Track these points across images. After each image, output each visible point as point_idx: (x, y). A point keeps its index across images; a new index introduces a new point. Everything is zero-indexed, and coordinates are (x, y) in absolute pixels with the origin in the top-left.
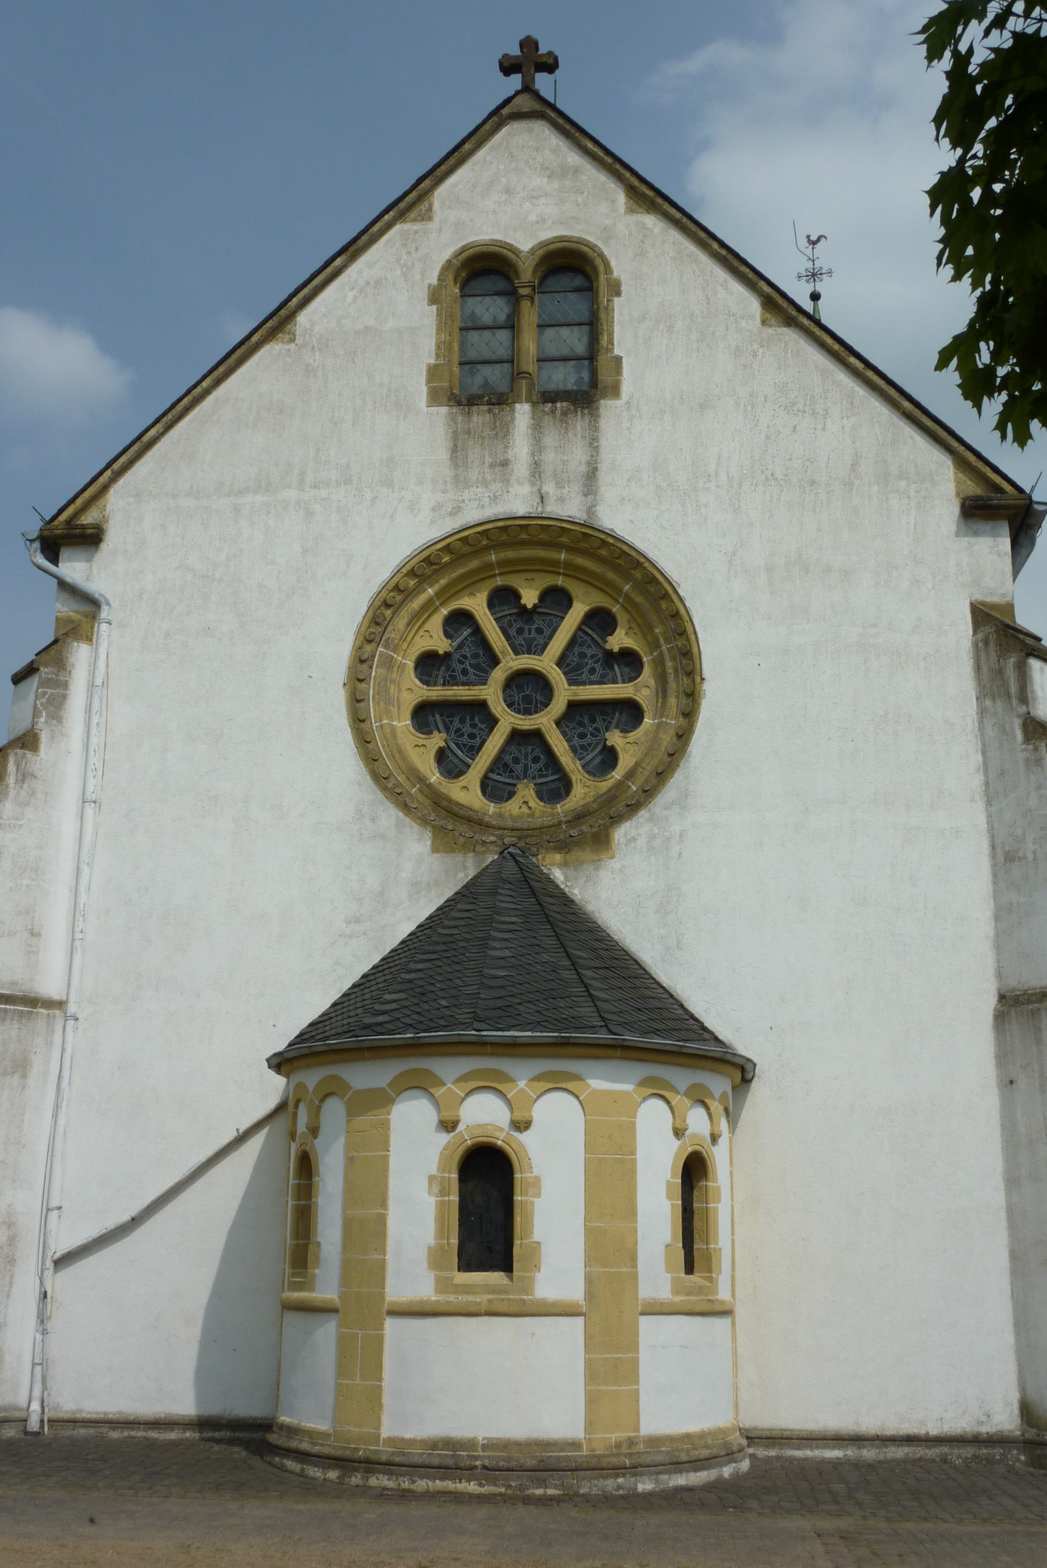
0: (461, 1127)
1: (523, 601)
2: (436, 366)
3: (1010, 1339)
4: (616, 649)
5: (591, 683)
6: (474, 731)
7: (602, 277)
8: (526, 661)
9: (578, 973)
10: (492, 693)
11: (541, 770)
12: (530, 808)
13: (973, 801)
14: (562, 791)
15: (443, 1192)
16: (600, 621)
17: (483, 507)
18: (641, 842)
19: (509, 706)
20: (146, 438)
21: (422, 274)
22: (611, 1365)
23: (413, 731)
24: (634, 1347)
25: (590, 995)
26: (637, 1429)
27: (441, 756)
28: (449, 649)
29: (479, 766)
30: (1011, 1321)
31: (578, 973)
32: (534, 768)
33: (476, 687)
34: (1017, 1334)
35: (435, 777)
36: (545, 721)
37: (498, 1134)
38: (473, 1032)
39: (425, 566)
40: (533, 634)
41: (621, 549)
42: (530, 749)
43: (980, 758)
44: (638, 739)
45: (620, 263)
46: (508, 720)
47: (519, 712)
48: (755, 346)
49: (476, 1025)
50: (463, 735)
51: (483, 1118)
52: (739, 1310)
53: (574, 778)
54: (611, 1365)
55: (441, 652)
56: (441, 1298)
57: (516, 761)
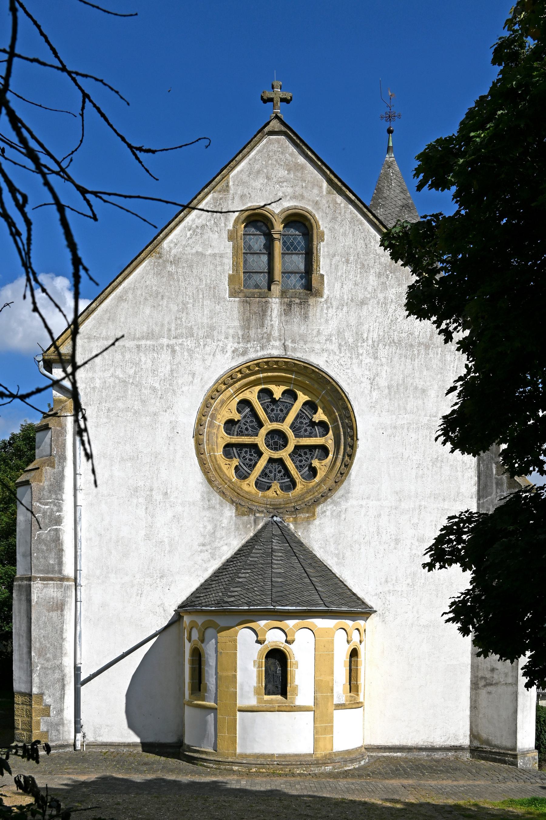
0: (266, 642)
1: (274, 397)
2: (233, 275)
3: (468, 712)
4: (317, 421)
5: (305, 437)
6: (252, 458)
7: (315, 231)
8: (275, 426)
9: (310, 580)
10: (260, 440)
11: (282, 476)
12: (277, 494)
13: (472, 498)
14: (292, 486)
15: (259, 667)
16: (311, 406)
17: (257, 351)
18: (328, 513)
19: (267, 446)
20: (90, 308)
21: (225, 224)
22: (323, 728)
23: (224, 457)
24: (331, 721)
25: (316, 590)
26: (332, 750)
27: (237, 468)
28: (240, 419)
29: (255, 474)
30: (469, 706)
31: (310, 580)
32: (279, 475)
33: (253, 437)
34: (471, 711)
35: (234, 479)
36: (284, 454)
37: (281, 645)
38: (272, 607)
39: (229, 379)
40: (279, 412)
41: (322, 375)
42: (277, 466)
43: (476, 478)
44: (327, 463)
45: (323, 223)
46: (267, 454)
47: (272, 449)
48: (388, 273)
49: (274, 604)
50: (246, 459)
51: (275, 639)
52: (366, 704)
53: (297, 481)
54: (323, 728)
55: (236, 420)
56: (259, 705)
57: (271, 472)
